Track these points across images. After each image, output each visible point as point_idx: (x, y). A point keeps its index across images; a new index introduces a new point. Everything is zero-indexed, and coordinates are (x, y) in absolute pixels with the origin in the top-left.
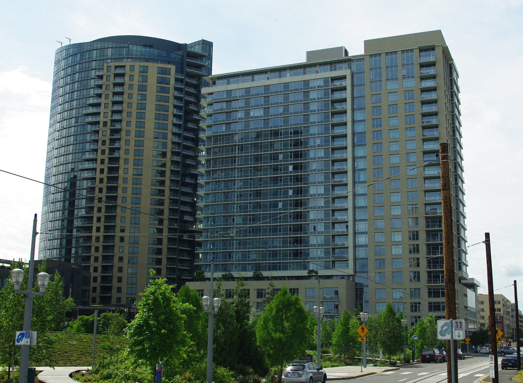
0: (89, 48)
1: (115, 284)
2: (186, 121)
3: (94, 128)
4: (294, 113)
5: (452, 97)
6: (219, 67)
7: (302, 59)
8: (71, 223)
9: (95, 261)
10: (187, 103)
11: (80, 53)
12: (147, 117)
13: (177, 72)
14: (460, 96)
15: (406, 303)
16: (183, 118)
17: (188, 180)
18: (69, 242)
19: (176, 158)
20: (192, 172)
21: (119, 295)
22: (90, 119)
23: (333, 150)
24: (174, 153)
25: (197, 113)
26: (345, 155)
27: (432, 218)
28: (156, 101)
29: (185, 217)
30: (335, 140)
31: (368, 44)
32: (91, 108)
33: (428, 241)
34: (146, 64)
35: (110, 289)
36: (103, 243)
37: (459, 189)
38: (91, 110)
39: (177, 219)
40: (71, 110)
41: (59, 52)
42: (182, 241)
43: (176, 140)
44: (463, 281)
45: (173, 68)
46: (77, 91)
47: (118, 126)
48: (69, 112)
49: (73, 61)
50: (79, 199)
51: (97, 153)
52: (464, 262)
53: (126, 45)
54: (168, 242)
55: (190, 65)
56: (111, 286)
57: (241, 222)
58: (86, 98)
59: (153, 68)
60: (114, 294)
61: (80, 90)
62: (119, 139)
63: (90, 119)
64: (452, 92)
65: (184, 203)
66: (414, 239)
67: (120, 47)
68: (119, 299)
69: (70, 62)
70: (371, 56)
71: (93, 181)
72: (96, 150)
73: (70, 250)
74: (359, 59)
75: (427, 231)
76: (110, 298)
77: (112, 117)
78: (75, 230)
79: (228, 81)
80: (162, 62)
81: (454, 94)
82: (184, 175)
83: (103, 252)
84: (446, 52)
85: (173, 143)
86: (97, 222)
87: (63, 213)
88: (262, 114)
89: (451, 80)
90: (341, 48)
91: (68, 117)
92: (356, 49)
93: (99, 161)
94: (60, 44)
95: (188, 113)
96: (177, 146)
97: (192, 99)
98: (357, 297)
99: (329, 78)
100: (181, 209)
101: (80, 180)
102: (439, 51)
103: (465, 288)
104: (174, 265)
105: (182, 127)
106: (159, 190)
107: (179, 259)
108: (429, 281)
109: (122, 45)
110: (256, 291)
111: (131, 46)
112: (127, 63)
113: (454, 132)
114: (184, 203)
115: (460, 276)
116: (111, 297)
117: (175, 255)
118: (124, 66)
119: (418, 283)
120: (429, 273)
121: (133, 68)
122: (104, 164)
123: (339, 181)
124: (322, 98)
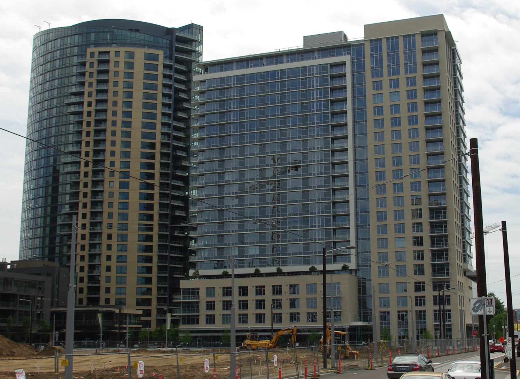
0: (70, 32)
1: (103, 284)
2: (176, 110)
3: (77, 119)
4: (293, 189)
5: (455, 83)
6: (212, 50)
7: (298, 44)
8: (54, 220)
9: (81, 250)
10: (177, 91)
11: (61, 38)
12: (128, 260)
13: (165, 57)
14: (463, 82)
15: (409, 283)
16: (172, 106)
17: (180, 114)
18: (52, 240)
19: (167, 91)
20: (183, 164)
21: (108, 296)
22: (73, 109)
23: (333, 139)
24: (163, 145)
25: (188, 101)
26: (345, 145)
27: (436, 209)
28: (144, 69)
29: (176, 232)
30: (335, 129)
31: (368, 28)
32: (73, 97)
33: (432, 233)
34: (132, 49)
35: (98, 289)
36: (94, 137)
37: (462, 178)
38: (73, 99)
39: (168, 173)
40: (53, 80)
41: (37, 37)
42: (175, 239)
43: (166, 120)
44: (467, 274)
45: (161, 54)
46: (59, 69)
47: (102, 117)
48: (49, 101)
49: (53, 47)
50: (62, 194)
51: (81, 145)
52: (469, 253)
53: (111, 30)
54: (160, 197)
55: (178, 50)
56: (99, 287)
57: (237, 228)
58: (68, 86)
59: (140, 54)
60: (103, 295)
61: (62, 68)
62: (105, 121)
63: (73, 109)
64: (455, 78)
65: (175, 198)
66: (418, 245)
67: (104, 32)
68: (107, 301)
69: (50, 48)
70: (371, 41)
71: (78, 175)
72: (80, 143)
73: (54, 249)
74: (358, 46)
75: (431, 237)
76: (98, 300)
77: (96, 106)
78: (58, 228)
79: (221, 67)
80: (150, 46)
81: (457, 92)
82: (173, 229)
83: (91, 219)
84: (448, 36)
85: (163, 134)
86: (83, 208)
87: (44, 230)
88: (258, 253)
89: (454, 66)
90: (340, 33)
91: (51, 79)
92: (355, 34)
93: (83, 154)
94: (38, 28)
95: (178, 101)
96: (166, 136)
97: (183, 87)
98: (359, 291)
99: (327, 64)
100: (172, 203)
101: (63, 174)
102: (441, 38)
103: (470, 280)
104: (166, 263)
105: (172, 116)
106: (146, 278)
107: (171, 257)
108: (434, 274)
109: (107, 30)
110: (254, 289)
111: (115, 30)
112: (112, 49)
113: (458, 132)
114: (175, 198)
115: (465, 268)
116: (99, 298)
117: (166, 252)
118: (109, 52)
119: (423, 276)
120: (433, 266)
121: (117, 54)
122: (86, 218)
123: (342, 212)
124: (321, 148)
